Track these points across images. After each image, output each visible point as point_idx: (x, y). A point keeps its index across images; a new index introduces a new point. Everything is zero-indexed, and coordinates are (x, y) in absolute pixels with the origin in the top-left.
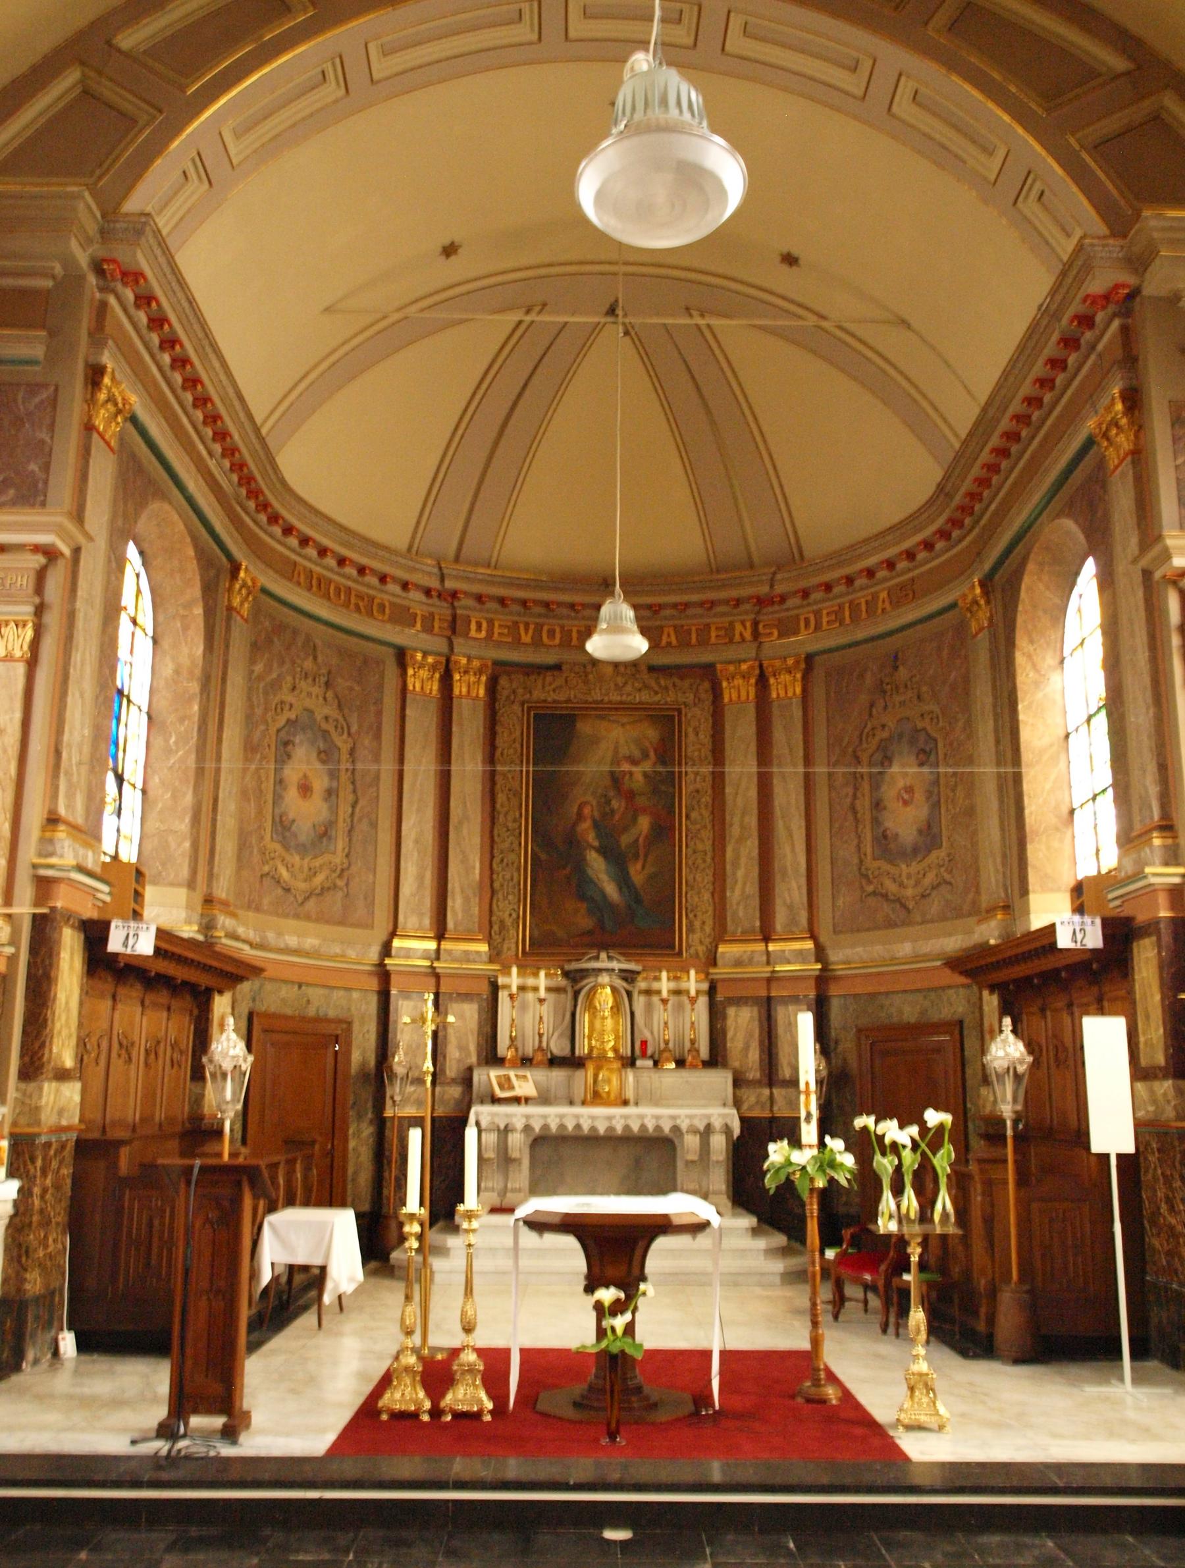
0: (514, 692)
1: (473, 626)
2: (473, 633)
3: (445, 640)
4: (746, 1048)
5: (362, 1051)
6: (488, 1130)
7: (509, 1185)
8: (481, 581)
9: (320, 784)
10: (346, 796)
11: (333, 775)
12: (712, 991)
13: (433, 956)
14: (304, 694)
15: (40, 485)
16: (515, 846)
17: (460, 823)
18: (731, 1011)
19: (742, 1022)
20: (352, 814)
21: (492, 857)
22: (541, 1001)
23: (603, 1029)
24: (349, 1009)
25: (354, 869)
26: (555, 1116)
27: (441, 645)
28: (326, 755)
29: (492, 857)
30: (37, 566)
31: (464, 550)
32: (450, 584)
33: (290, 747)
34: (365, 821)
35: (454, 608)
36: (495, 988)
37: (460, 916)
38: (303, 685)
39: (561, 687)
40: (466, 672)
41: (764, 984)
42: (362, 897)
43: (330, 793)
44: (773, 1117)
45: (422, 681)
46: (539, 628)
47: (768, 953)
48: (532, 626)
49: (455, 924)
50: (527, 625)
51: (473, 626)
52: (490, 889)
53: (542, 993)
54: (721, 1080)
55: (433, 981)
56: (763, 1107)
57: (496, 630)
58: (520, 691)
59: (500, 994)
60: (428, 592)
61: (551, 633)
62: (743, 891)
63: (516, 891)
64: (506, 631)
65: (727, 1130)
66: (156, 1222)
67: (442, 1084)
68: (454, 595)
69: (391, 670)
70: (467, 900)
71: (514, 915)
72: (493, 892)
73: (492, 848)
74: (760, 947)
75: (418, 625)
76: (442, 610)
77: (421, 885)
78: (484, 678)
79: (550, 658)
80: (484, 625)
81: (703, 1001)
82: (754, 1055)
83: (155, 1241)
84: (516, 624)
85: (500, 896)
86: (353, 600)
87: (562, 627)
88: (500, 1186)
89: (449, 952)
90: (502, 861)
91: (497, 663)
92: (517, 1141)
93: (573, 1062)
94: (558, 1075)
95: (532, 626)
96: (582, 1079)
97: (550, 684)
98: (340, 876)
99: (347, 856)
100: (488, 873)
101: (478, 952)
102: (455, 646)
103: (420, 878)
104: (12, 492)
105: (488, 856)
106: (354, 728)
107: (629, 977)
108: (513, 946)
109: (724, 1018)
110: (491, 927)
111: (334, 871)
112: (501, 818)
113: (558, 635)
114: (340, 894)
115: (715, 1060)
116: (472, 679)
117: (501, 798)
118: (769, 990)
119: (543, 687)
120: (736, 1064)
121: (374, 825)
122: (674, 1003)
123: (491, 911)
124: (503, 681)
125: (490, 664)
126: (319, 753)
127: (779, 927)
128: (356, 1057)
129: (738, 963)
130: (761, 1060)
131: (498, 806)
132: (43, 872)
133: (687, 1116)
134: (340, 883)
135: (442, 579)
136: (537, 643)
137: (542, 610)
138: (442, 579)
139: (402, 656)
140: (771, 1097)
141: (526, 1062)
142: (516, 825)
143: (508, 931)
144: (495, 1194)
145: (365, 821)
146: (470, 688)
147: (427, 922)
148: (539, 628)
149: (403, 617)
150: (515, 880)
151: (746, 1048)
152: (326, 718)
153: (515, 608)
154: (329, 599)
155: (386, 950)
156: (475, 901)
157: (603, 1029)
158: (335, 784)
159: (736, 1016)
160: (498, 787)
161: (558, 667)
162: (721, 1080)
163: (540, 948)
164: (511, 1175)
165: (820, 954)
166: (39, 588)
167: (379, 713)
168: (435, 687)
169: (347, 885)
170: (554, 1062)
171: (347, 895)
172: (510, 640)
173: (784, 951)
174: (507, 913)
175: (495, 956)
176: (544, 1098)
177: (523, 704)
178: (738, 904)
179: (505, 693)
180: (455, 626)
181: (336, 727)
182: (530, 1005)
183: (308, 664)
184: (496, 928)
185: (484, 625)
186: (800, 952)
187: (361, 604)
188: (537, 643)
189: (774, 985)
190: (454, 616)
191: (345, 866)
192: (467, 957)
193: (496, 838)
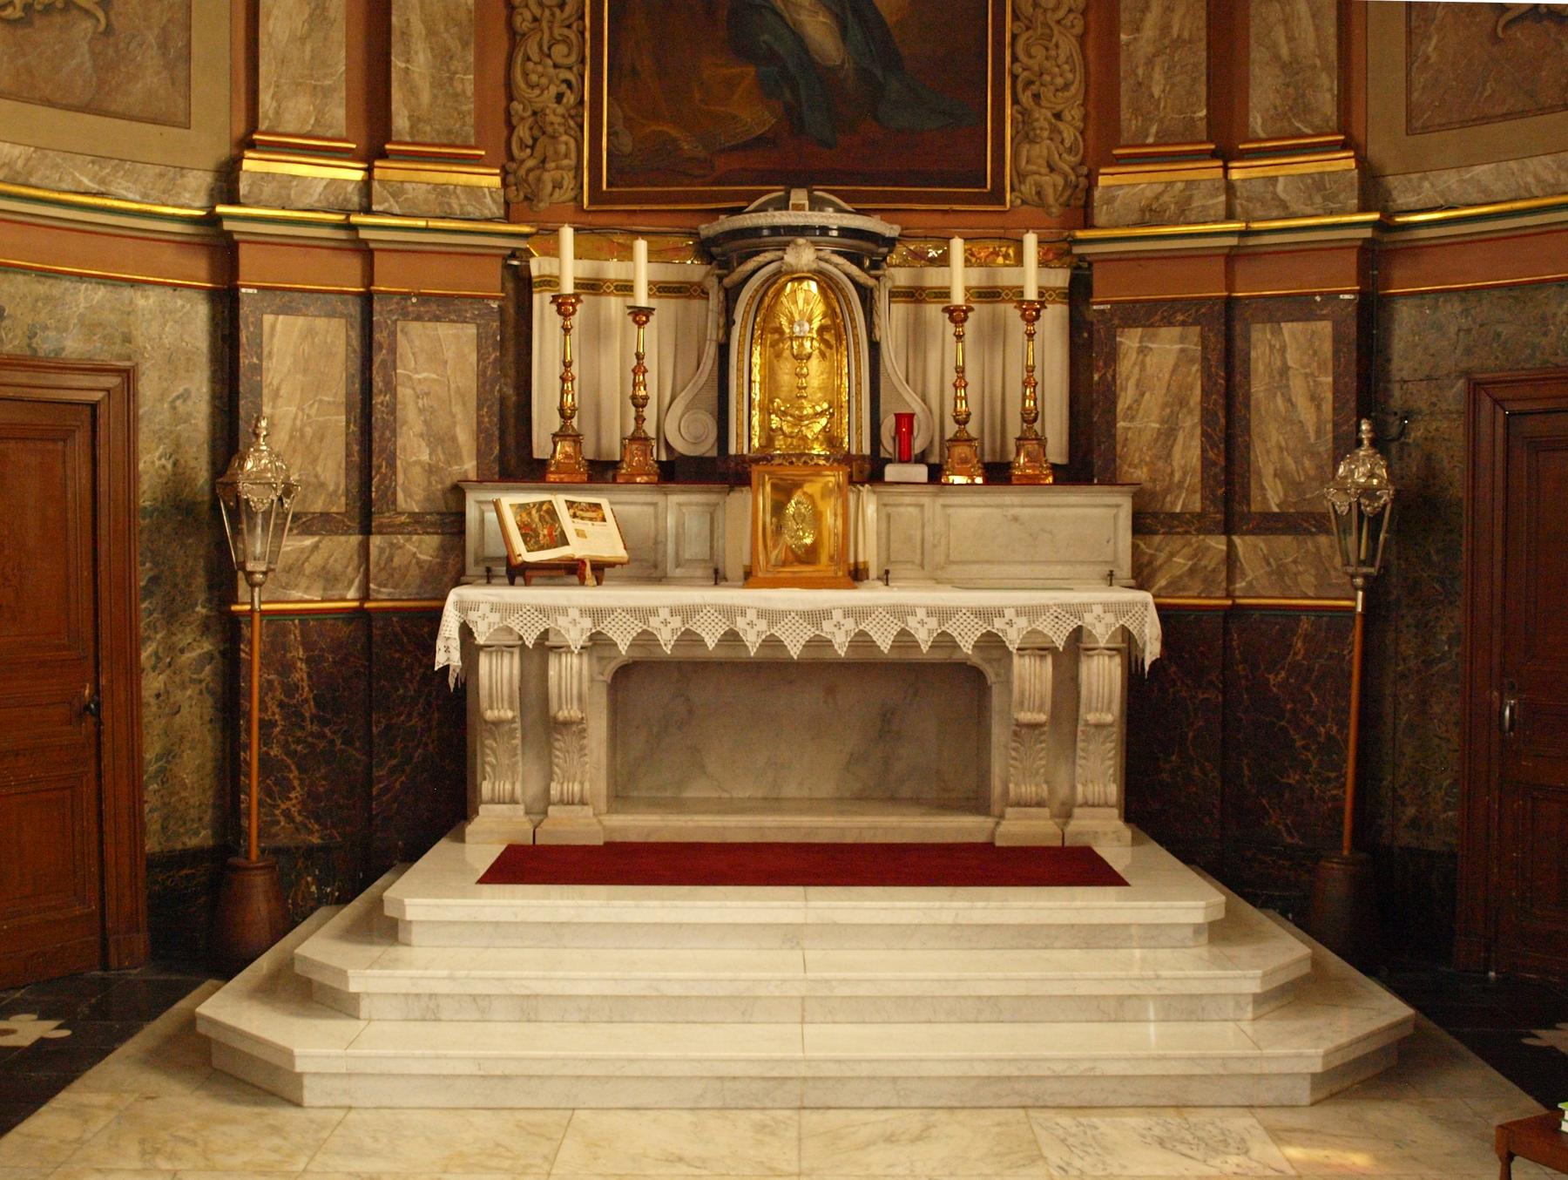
4: (1168, 433)
12: (1078, 293)
18: (1130, 340)
19: (1156, 367)
22: (640, 315)
23: (802, 380)
26: (670, 611)
36: (522, 285)
37: (426, 98)
41: (1220, 266)
44: (1235, 612)
47: (1230, 188)
49: (415, 120)
54: (1100, 515)
56: (1208, 582)
62: (1165, 29)
65: (1127, 645)
70: (443, 56)
72: (515, 38)
74: (1210, 172)
81: (1054, 317)
82: (1188, 453)
92: (570, 675)
93: (718, 471)
94: (680, 511)
96: (745, 509)
101: (472, 190)
107: (865, 250)
108: (568, 181)
109: (1112, 357)
115: (1086, 464)
118: (1230, 287)
120: (1141, 474)
122: (981, 323)
127: (1256, 122)
129: (1151, 214)
130: (1206, 463)
133: (1107, 607)
140: (1231, 558)
141: (602, 471)
147: (338, 115)
151: (1168, 433)
155: (227, 184)
157: (802, 380)
159: (1142, 351)
162: (1100, 515)
163: (629, 192)
164: (559, 758)
165: (1371, 189)
170: (674, 471)
173: (1274, 180)
174: (553, 90)
175: (519, 200)
176: (647, 565)
178: (1150, 63)
182: (612, 330)
186: (1318, 183)
189: (1240, 268)
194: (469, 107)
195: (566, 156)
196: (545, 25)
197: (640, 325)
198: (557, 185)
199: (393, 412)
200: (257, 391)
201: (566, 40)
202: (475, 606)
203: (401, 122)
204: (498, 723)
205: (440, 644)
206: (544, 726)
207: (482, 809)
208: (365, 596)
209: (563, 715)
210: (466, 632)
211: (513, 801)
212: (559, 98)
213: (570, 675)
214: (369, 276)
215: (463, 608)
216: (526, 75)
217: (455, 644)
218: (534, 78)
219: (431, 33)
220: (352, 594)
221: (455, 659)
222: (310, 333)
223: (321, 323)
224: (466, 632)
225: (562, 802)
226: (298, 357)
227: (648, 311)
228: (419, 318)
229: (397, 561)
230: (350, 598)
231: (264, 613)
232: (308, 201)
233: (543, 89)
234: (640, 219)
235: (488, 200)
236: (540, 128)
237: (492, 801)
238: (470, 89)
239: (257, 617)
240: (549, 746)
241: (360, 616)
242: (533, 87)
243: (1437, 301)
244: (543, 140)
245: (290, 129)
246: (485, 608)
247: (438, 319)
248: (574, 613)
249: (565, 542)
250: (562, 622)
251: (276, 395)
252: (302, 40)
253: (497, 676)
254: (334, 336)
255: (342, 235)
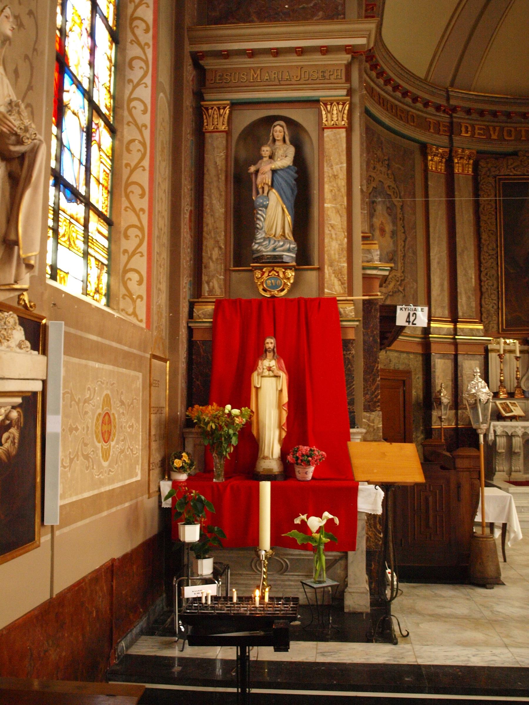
0: (489, 170)
1: (463, 129)
2: (463, 134)
3: (447, 138)
5: (416, 391)
6: (500, 436)
7: (513, 468)
8: (469, 100)
9: (389, 228)
10: (401, 236)
11: (394, 223)
13: (452, 332)
14: (378, 172)
15: (340, 8)
16: (494, 265)
17: (463, 251)
20: (404, 247)
21: (480, 272)
22: (517, 358)
24: (409, 365)
25: (407, 280)
27: (444, 140)
28: (390, 210)
29: (480, 272)
30: (345, 62)
31: (456, 81)
32: (453, 102)
33: (375, 204)
34: (410, 250)
35: (451, 117)
37: (465, 308)
38: (378, 166)
39: (518, 166)
40: (461, 158)
42: (411, 297)
43: (394, 234)
45: (435, 164)
46: (502, 129)
48: (497, 128)
49: (463, 313)
50: (494, 128)
51: (463, 129)
52: (480, 291)
53: (518, 354)
55: (452, 347)
57: (477, 131)
58: (493, 169)
59: (490, 354)
60: (438, 108)
61: (510, 133)
63: (496, 292)
64: (481, 132)
66: (430, 499)
67: (461, 409)
68: (454, 109)
69: (418, 157)
70: (469, 298)
71: (496, 307)
72: (482, 293)
73: (480, 266)
75: (432, 131)
76: (444, 118)
77: (442, 290)
78: (471, 161)
79: (509, 148)
80: (470, 129)
83: (431, 512)
84: (488, 127)
85: (487, 296)
86: (399, 113)
87: (515, 128)
88: (506, 468)
89: (462, 330)
90: (486, 274)
91: (478, 152)
92: (517, 442)
95: (497, 128)
97: (511, 164)
98: (400, 285)
99: (403, 272)
100: (478, 282)
101: (478, 330)
102: (454, 141)
103: (442, 285)
104: (321, 13)
105: (478, 272)
106: (402, 193)
108: (496, 326)
110: (482, 314)
111: (398, 281)
112: (485, 249)
113: (513, 133)
114: (401, 295)
116: (465, 162)
117: (484, 236)
119: (507, 166)
121: (415, 253)
123: (481, 306)
124: (482, 163)
125: (475, 152)
126: (388, 208)
128: (414, 393)
131: (483, 241)
132: (369, 272)
134: (401, 289)
135: (448, 99)
136: (501, 139)
137: (504, 118)
138: (448, 99)
139: (424, 148)
142: (494, 252)
143: (492, 317)
144: (505, 473)
145: (410, 250)
146: (463, 169)
147: (446, 312)
148: (502, 129)
149: (423, 125)
150: (495, 286)
152: (389, 186)
153: (488, 117)
154: (387, 110)
156: (473, 298)
158: (395, 228)
160: (482, 229)
161: (515, 154)
164: (513, 461)
166: (348, 79)
167: (414, 184)
168: (442, 167)
169: (404, 290)
171: (404, 296)
172: (484, 137)
174: (491, 305)
177: (495, 177)
179: (484, 171)
180: (452, 130)
181: (394, 192)
183: (379, 153)
184: (484, 315)
185: (470, 129)
187: (402, 115)
188: (501, 139)
190: (451, 123)
191: (403, 278)
192: (472, 332)
193: (482, 260)
194: (474, 310)
195: (495, 320)
196: (489, 290)
197: (517, 360)
198: (493, 327)
199: (462, 382)
200: (434, 378)
201: (494, 294)
202: (497, 426)
203: (460, 314)
204: (500, 453)
205: (490, 435)
206: (511, 452)
207: (497, 473)
208: (457, 424)
209: (516, 451)
210: (495, 432)
211: (503, 471)
212: (493, 307)
213: (517, 442)
214: (456, 350)
215: (494, 426)
216: (485, 302)
217: (493, 435)
218: (487, 302)
219: (466, 293)
220: (453, 424)
221: (493, 438)
222: (444, 363)
223: (446, 361)
224: (495, 432)
225: (515, 471)
226: (441, 367)
227: (519, 357)
228: (467, 360)
229: (464, 416)
230: (453, 426)
231: (444, 428)
232: (443, 333)
233: (490, 305)
234: (512, 335)
235: (481, 332)
236: (489, 314)
237: (499, 471)
238: (474, 305)
239: (443, 429)
240: (511, 459)
241: (456, 430)
242: (486, 304)
243: (443, 314)
244: (490, 317)
245: (437, 316)
246: (499, 426)
247: (471, 360)
248: (520, 428)
249: (512, 412)
250: (517, 430)
251: (438, 378)
252: (439, 295)
253: (501, 442)
254: (449, 364)
255: (452, 341)
